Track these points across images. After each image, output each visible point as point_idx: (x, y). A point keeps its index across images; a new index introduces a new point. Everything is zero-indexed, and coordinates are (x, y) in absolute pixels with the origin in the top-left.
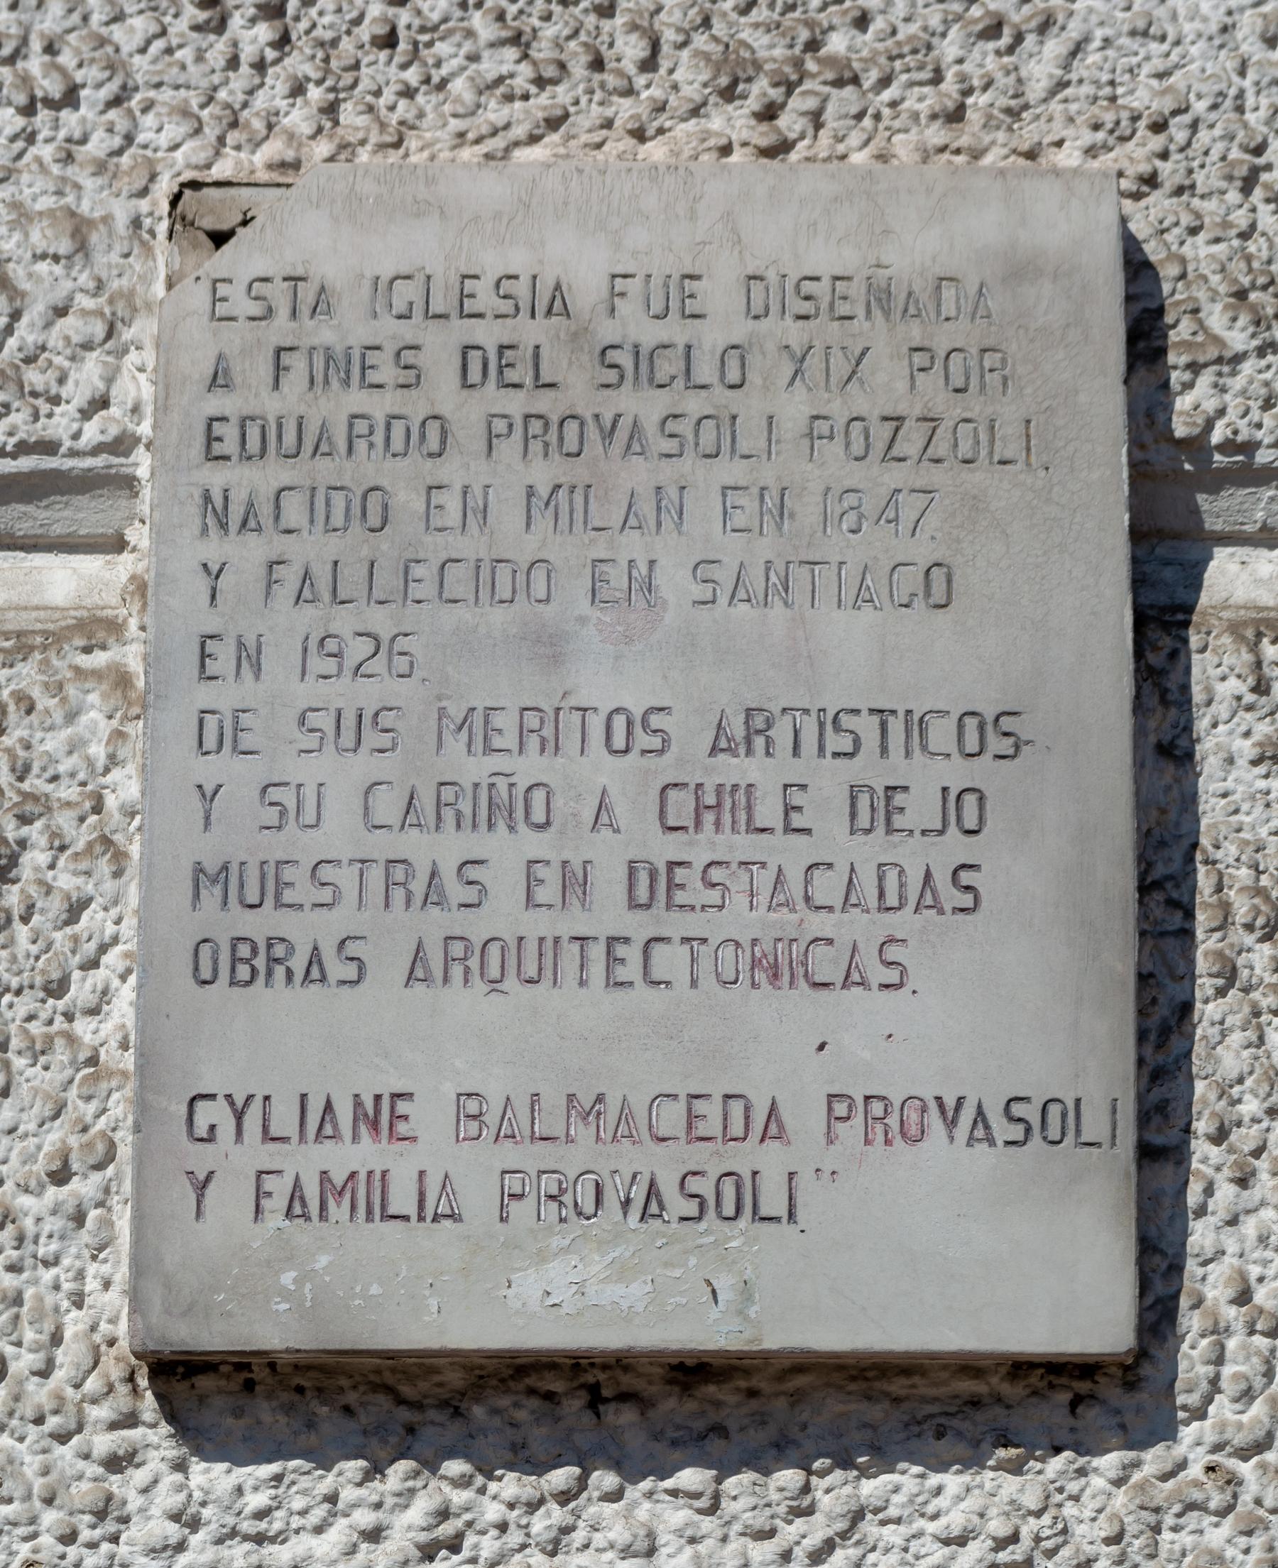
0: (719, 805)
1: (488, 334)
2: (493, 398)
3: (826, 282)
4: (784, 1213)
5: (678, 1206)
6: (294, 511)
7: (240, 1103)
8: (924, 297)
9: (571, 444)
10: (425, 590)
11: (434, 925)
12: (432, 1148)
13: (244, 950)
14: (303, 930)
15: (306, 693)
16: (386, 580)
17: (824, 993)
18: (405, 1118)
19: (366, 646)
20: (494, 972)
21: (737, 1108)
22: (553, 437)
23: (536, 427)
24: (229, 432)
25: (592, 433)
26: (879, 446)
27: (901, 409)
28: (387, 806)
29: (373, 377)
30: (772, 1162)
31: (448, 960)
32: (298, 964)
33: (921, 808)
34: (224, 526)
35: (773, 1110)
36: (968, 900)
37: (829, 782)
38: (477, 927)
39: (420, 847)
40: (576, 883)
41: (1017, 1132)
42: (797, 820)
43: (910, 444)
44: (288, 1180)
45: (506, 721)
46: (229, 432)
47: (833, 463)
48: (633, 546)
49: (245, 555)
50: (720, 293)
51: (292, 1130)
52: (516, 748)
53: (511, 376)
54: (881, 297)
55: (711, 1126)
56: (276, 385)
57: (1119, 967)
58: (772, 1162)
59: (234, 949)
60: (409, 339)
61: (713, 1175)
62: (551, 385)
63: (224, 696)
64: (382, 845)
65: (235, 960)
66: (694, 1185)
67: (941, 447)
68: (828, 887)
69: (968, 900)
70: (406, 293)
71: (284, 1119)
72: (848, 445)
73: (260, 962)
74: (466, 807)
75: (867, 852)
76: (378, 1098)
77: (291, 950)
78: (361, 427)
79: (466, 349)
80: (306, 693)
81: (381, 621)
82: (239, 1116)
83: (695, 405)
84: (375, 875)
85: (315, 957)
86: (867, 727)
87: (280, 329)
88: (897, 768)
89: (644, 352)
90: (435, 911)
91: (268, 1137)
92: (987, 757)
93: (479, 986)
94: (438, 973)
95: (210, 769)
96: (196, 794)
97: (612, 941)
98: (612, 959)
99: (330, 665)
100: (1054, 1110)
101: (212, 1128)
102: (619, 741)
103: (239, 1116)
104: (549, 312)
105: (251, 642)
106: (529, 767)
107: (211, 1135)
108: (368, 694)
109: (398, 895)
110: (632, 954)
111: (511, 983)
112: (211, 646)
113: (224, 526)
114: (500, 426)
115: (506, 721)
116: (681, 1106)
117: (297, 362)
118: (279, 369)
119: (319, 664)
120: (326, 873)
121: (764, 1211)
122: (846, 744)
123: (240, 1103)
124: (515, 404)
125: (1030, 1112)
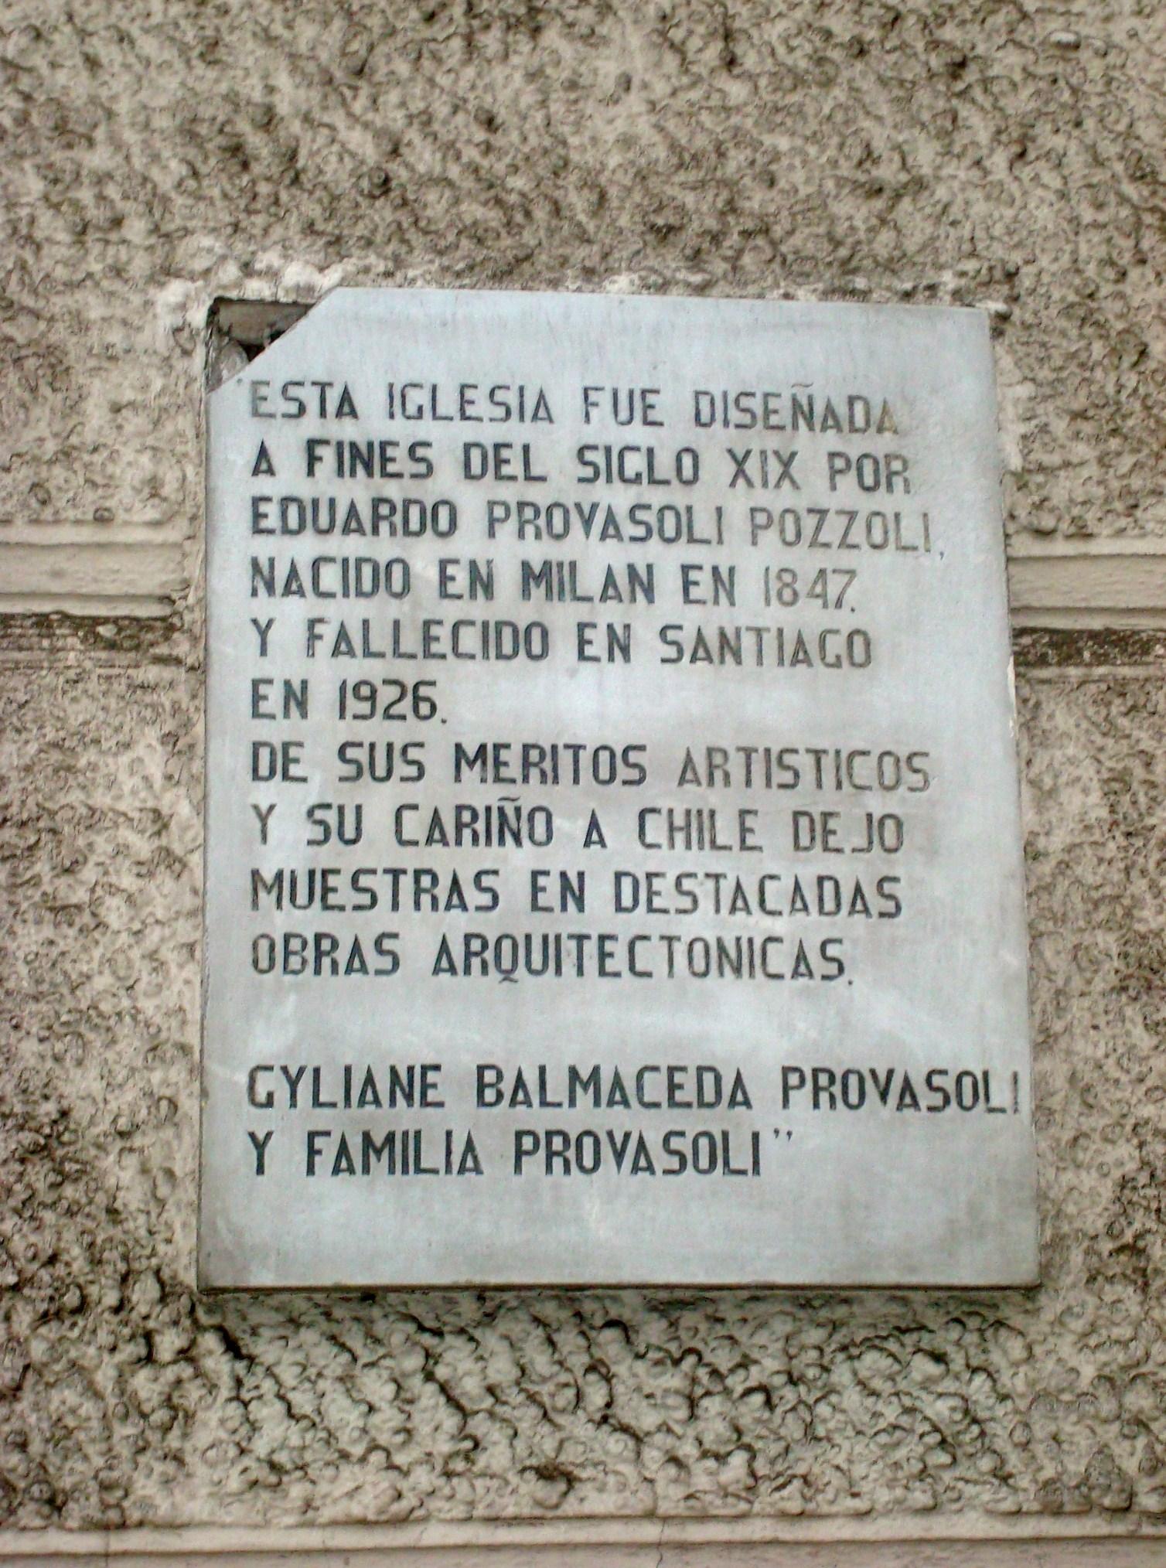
0: (688, 825)
1: (488, 434)
2: (490, 488)
3: (759, 397)
4: (749, 1166)
5: (662, 1160)
6: (330, 577)
7: (293, 1072)
8: (842, 410)
9: (558, 526)
10: (443, 646)
11: (457, 924)
12: (457, 1112)
13: (295, 945)
14: (344, 927)
15: (348, 730)
16: (411, 641)
17: (774, 983)
18: (434, 1086)
19: (393, 692)
20: (506, 964)
21: (709, 1078)
22: (542, 521)
23: (529, 513)
24: (272, 510)
25: (574, 517)
26: (808, 532)
27: (823, 504)
28: (415, 825)
29: (391, 468)
30: (739, 1124)
31: (468, 954)
32: (342, 955)
33: (849, 833)
34: (270, 587)
35: (739, 1080)
36: (890, 906)
37: (774, 808)
38: (490, 926)
39: (443, 860)
40: (573, 891)
41: (937, 1099)
42: (751, 840)
43: (832, 531)
44: (335, 1139)
45: (513, 757)
46: (272, 510)
47: (770, 551)
48: (610, 613)
49: (290, 614)
50: (675, 405)
51: (339, 1097)
52: (519, 778)
53: (506, 470)
54: (803, 412)
55: (688, 1094)
56: (311, 472)
57: (229, 650)
58: (739, 1124)
59: (467, 945)
60: (421, 436)
61: (690, 1137)
62: (542, 479)
63: (275, 732)
64: (410, 859)
65: (287, 953)
66: (675, 1143)
67: (857, 535)
68: (778, 894)
69: (890, 906)
70: (418, 398)
71: (331, 1091)
72: (782, 531)
73: (310, 953)
74: (480, 826)
75: (811, 866)
76: (411, 1069)
77: (335, 944)
78: (384, 510)
79: (468, 447)
80: (348, 730)
81: (409, 672)
82: (293, 1084)
83: (657, 497)
84: (406, 882)
85: (356, 949)
86: (804, 762)
87: (312, 426)
88: (828, 799)
89: (844, 756)
90: (456, 912)
91: (317, 1103)
92: (902, 790)
93: (494, 974)
94: (459, 964)
95: (266, 793)
96: (252, 813)
97: (602, 938)
98: (603, 955)
99: (365, 708)
100: (967, 1082)
101: (270, 1095)
102: (604, 774)
103: (293, 1084)
104: (535, 417)
105: (297, 686)
106: (531, 794)
107: (269, 1102)
108: (398, 733)
109: (426, 899)
110: (619, 949)
111: (521, 971)
112: (263, 689)
113: (270, 587)
114: (499, 512)
115: (513, 757)
116: (663, 1075)
117: (327, 454)
118: (312, 460)
119: (354, 706)
120: (364, 881)
121: (733, 1165)
122: (788, 777)
123: (293, 1072)
124: (510, 493)
125: (948, 1083)
